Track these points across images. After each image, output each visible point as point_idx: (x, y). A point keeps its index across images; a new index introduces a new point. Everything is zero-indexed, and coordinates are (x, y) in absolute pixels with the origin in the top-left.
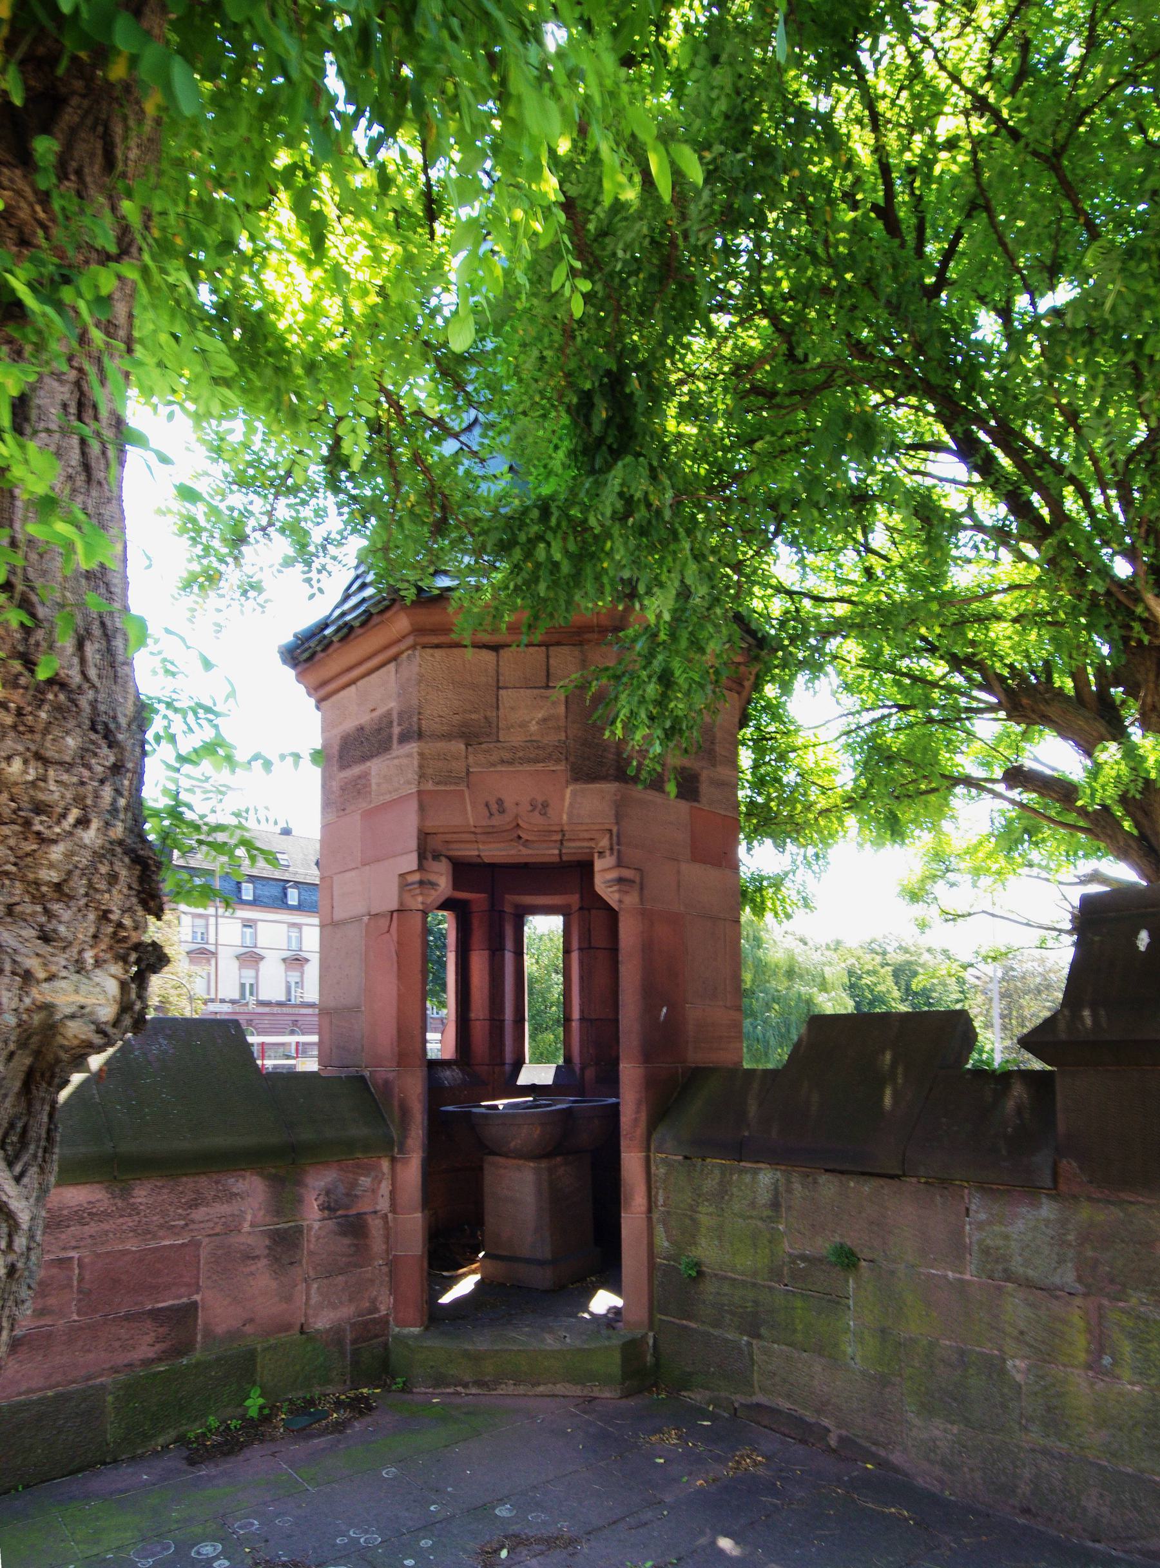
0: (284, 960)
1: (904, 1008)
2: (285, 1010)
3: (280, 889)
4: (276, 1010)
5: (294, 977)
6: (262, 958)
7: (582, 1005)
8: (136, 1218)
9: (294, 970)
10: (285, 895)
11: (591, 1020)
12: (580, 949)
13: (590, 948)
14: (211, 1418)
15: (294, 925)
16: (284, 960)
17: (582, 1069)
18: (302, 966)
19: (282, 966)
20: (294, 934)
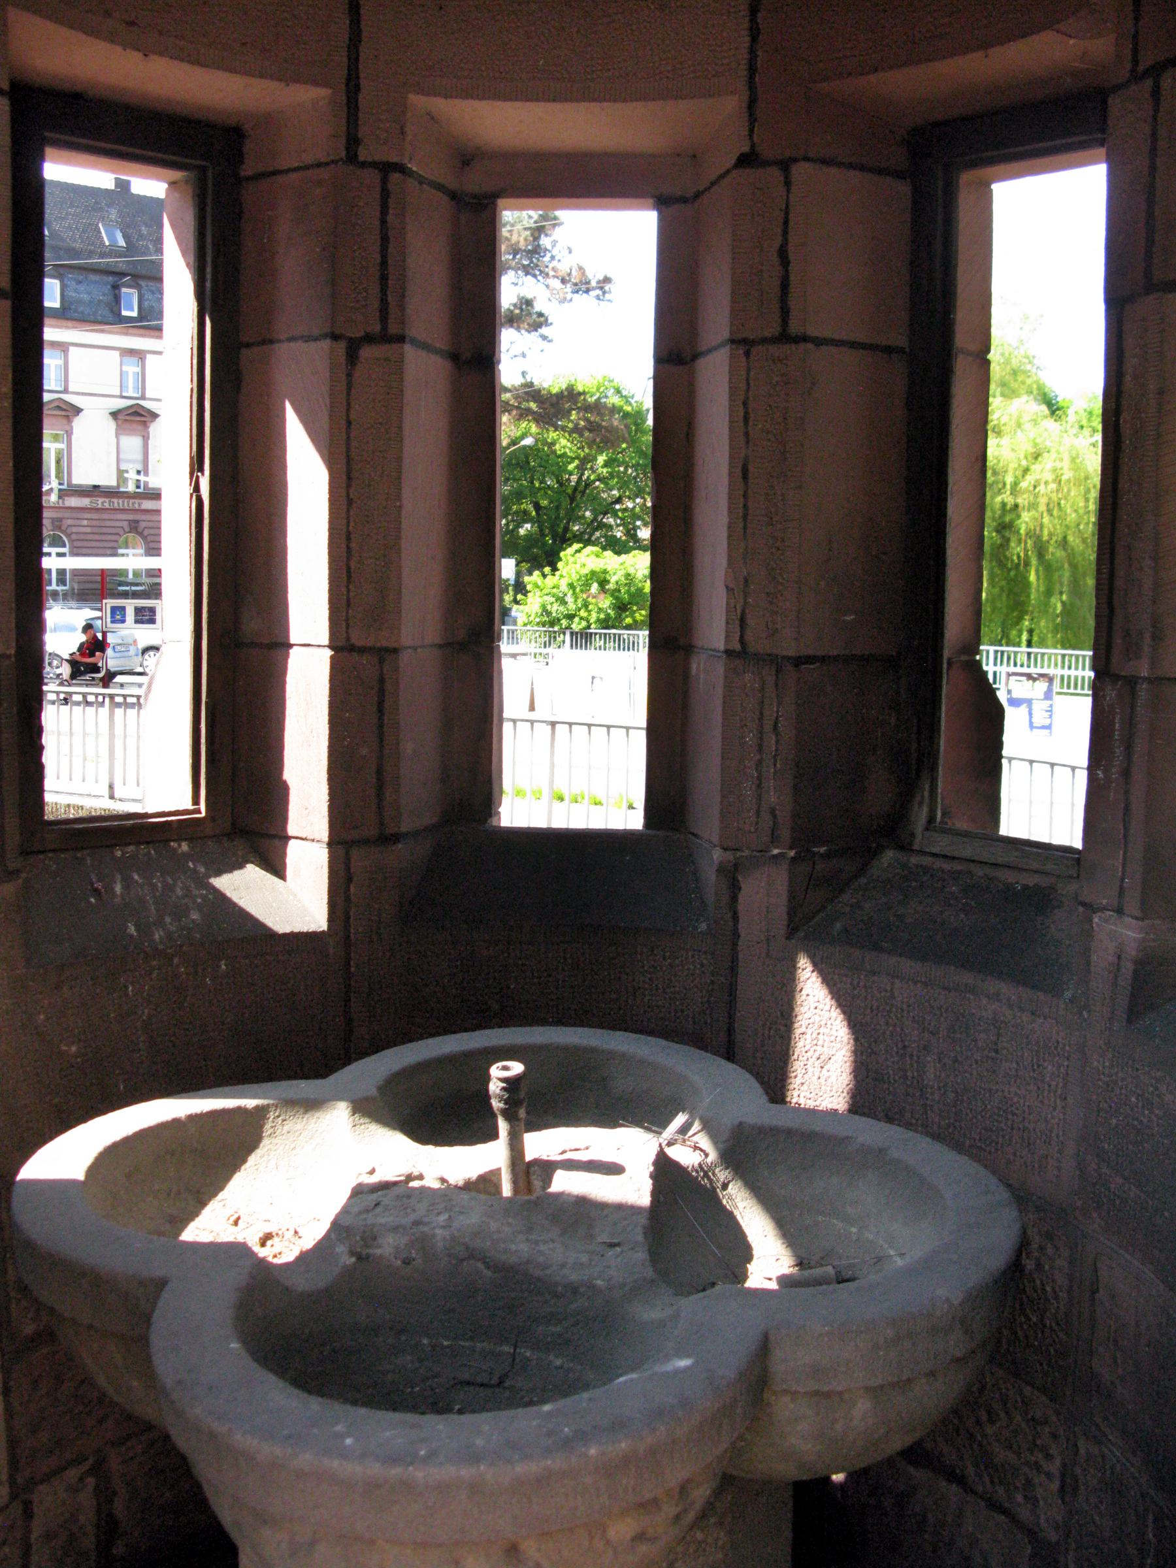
0: (115, 415)
1: (44, 490)
2: (117, 503)
3: (107, 289)
4: (101, 502)
5: (132, 443)
6: (77, 411)
7: (740, 588)
8: (928, 1018)
9: (131, 432)
10: (117, 299)
11: (776, 662)
12: (742, 344)
13: (784, 337)
14: (834, 1477)
15: (131, 352)
16: (115, 415)
17: (732, 876)
18: (145, 425)
19: (111, 425)
20: (132, 369)
